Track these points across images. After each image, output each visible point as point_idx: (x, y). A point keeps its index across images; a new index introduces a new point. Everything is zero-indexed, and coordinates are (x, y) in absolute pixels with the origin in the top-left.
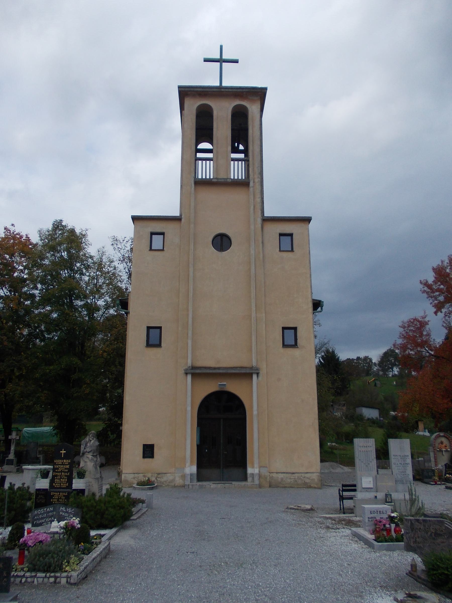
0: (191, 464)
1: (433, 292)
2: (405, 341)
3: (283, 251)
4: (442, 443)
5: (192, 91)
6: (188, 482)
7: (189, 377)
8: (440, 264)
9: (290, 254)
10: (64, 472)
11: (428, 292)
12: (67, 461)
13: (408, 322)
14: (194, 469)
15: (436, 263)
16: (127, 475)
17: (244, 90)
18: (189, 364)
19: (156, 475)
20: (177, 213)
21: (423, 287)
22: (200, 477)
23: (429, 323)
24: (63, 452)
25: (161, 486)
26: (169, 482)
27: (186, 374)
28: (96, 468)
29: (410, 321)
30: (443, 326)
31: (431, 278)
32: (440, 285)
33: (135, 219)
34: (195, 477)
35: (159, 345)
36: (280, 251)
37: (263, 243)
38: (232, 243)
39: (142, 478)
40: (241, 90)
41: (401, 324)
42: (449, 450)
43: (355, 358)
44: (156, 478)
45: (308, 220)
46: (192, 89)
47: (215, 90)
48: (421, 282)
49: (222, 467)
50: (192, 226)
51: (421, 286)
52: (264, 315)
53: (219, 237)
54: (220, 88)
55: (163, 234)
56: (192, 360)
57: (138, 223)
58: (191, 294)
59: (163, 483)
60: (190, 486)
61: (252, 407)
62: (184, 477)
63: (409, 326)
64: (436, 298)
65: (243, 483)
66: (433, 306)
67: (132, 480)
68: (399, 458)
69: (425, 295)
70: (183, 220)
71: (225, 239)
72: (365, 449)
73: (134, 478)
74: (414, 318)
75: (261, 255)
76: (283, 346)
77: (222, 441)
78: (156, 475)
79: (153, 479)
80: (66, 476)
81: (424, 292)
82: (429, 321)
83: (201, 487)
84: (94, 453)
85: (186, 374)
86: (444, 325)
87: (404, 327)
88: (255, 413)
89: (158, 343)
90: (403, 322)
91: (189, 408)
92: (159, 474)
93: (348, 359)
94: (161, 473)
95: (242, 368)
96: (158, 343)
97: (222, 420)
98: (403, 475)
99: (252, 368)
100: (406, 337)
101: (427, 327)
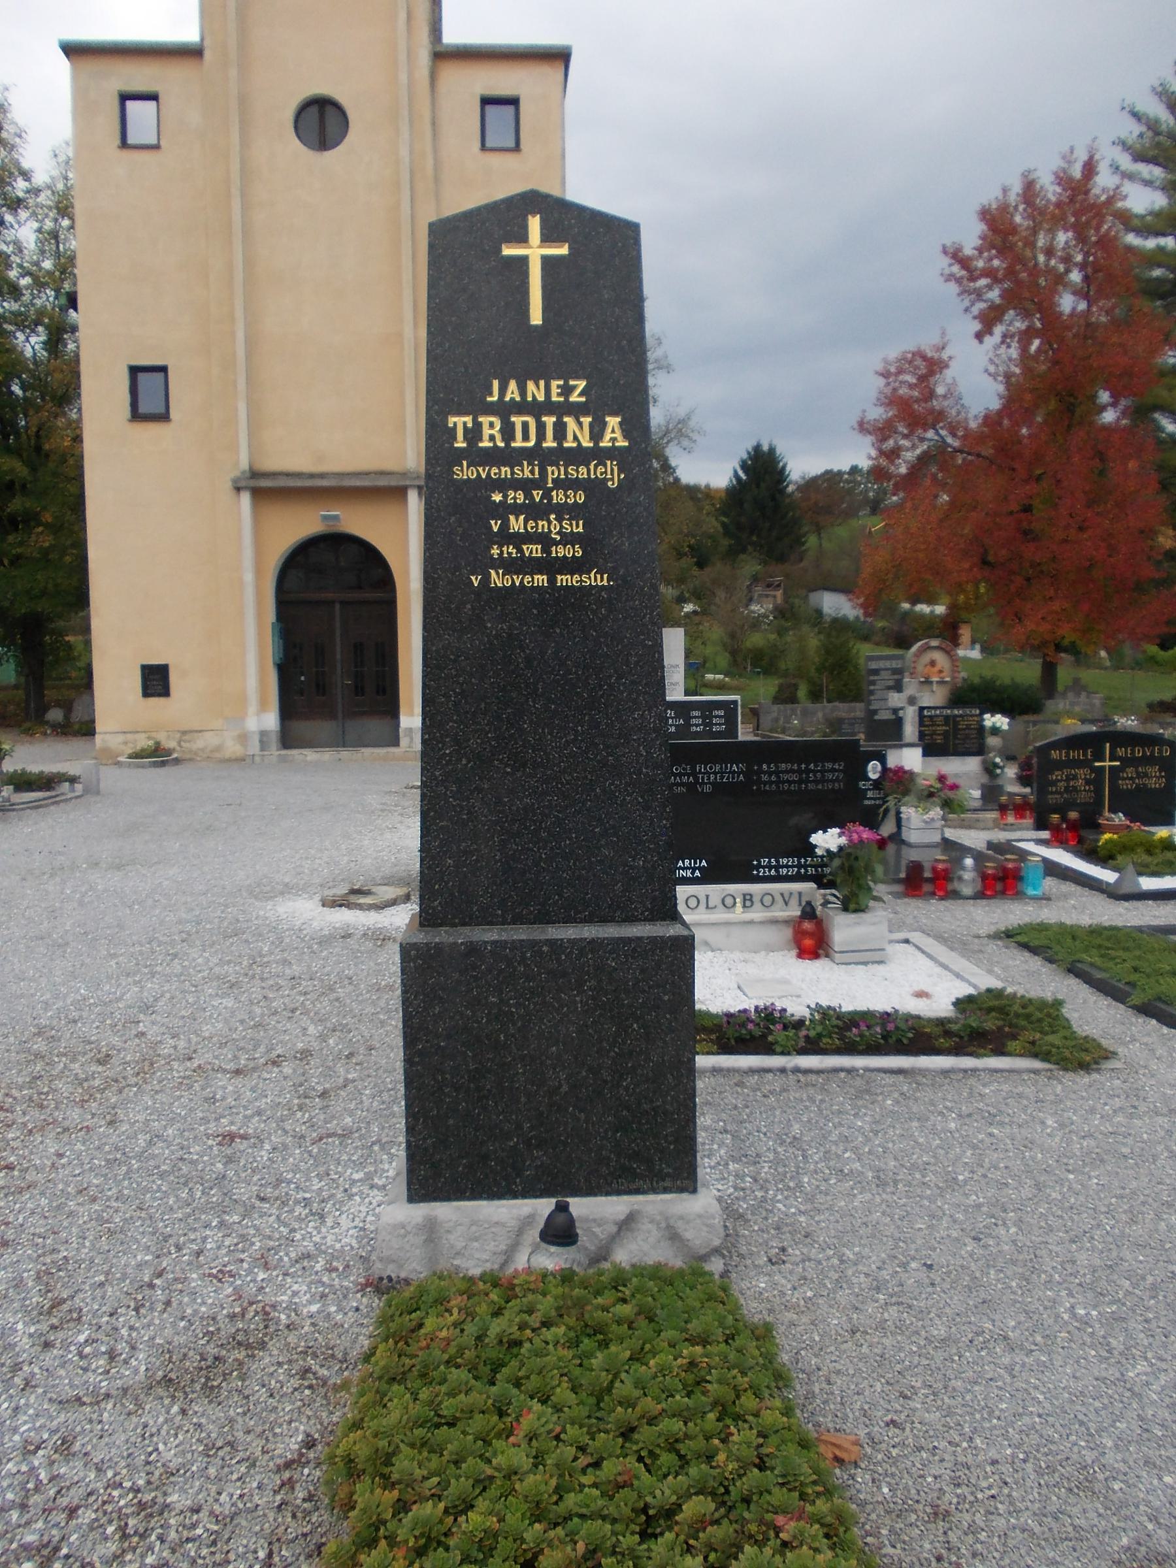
0: (263, 706)
1: (973, 279)
2: (890, 414)
4: (933, 663)
6: (254, 747)
7: (246, 499)
8: (1001, 197)
9: (510, 160)
11: (962, 278)
13: (899, 360)
14: (271, 720)
15: (990, 196)
16: (107, 737)
18: (244, 464)
19: (178, 735)
20: (190, 34)
21: (950, 265)
22: (288, 739)
23: (952, 363)
25: (191, 760)
26: (212, 751)
27: (238, 489)
29: (904, 359)
30: (986, 371)
31: (970, 235)
32: (991, 259)
33: (72, 50)
34: (274, 740)
35: (164, 417)
36: (483, 147)
37: (434, 124)
38: (351, 124)
39: (143, 742)
41: (880, 367)
42: (948, 679)
43: (846, 468)
45: (560, 57)
48: (945, 251)
49: (340, 715)
50: (233, 72)
51: (946, 261)
53: (314, 110)
55: (153, 97)
56: (251, 454)
57: (92, 65)
58: (239, 276)
60: (257, 759)
61: (407, 572)
62: (243, 738)
63: (900, 371)
64: (979, 294)
65: (393, 750)
66: (975, 318)
67: (123, 747)
69: (953, 288)
70: (207, 54)
71: (330, 110)
73: (126, 743)
74: (916, 349)
75: (430, 162)
77: (338, 656)
78: (178, 735)
79: (171, 744)
81: (950, 277)
82: (950, 358)
83: (282, 759)
85: (238, 489)
86: (992, 369)
87: (885, 375)
89: (163, 410)
90: (885, 361)
91: (249, 577)
92: (184, 733)
93: (827, 472)
94: (191, 732)
95: (382, 473)
96: (163, 410)
97: (337, 606)
99: (404, 475)
100: (893, 400)
101: (949, 374)
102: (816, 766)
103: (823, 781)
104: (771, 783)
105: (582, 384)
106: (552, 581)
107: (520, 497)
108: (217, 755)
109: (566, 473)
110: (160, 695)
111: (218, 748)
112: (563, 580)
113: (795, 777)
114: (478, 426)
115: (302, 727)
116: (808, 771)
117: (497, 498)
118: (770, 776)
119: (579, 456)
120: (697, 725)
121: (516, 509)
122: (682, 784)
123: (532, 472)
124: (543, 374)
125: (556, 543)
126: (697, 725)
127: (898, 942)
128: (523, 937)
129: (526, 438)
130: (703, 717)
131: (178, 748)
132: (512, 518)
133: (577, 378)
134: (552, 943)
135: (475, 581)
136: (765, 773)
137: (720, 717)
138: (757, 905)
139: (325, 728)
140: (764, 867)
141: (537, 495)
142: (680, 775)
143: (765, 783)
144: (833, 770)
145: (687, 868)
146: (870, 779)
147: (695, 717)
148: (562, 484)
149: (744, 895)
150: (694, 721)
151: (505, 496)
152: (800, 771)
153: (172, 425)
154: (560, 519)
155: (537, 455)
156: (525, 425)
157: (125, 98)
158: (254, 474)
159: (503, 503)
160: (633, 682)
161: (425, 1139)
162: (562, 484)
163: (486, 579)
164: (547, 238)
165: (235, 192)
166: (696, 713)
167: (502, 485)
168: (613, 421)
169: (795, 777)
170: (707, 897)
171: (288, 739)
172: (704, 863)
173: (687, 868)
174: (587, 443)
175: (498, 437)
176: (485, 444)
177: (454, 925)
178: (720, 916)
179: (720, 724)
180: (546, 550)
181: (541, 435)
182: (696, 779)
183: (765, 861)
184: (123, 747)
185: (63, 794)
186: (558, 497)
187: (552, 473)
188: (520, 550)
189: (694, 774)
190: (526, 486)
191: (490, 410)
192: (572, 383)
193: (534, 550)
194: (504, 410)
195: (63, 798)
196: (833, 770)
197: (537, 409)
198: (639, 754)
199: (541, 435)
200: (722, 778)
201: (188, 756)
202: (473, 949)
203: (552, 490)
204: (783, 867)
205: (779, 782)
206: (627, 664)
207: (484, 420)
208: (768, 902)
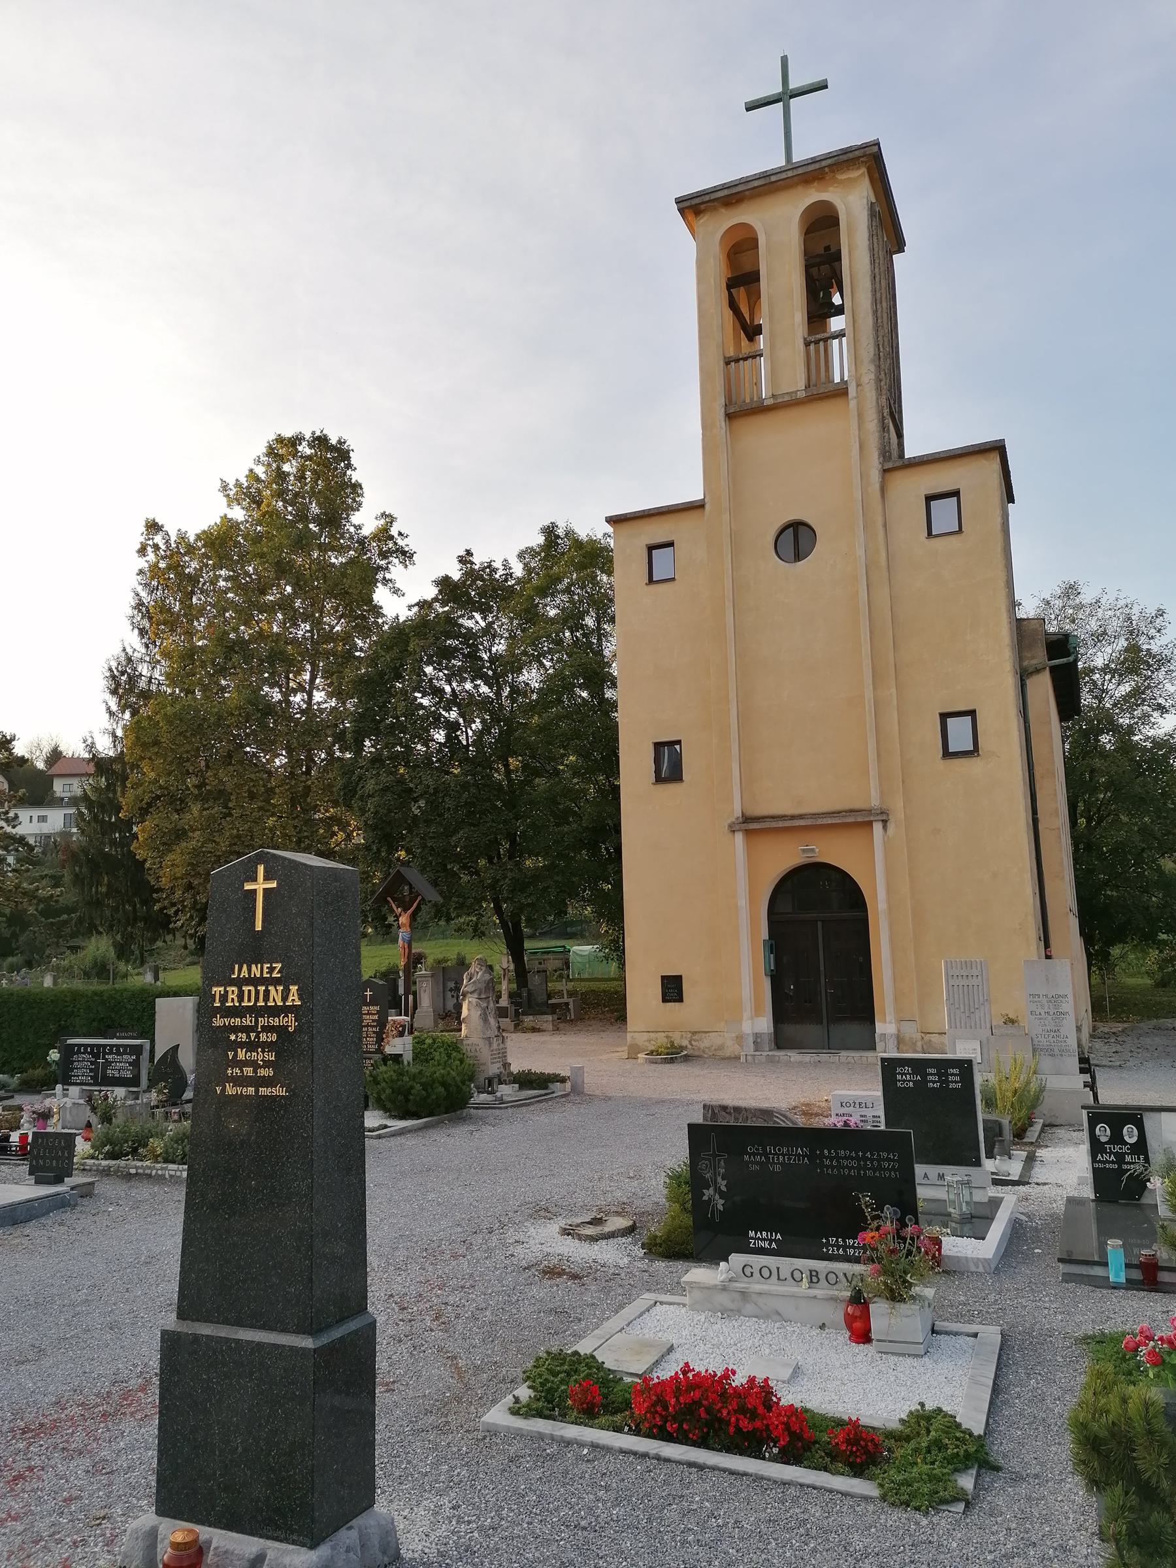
0: (757, 1012)
3: (658, 582)
5: (708, 202)
7: (739, 838)
10: (371, 1026)
12: (375, 1008)
14: (765, 1024)
17: (824, 163)
20: (695, 493)
22: (780, 1041)
24: (368, 993)
26: (715, 1050)
28: (485, 1020)
34: (767, 1043)
37: (885, 525)
40: (817, 166)
44: (690, 1042)
46: (707, 198)
47: (756, 184)
49: (825, 1021)
52: (894, 690)
54: (790, 166)
57: (626, 528)
59: (704, 1052)
62: (740, 1039)
67: (647, 1044)
68: (1045, 1000)
70: (707, 507)
71: (802, 529)
72: (965, 982)
73: (649, 1041)
75: (884, 555)
76: (944, 756)
80: (374, 1032)
83: (771, 1060)
84: (480, 995)
88: (882, 906)
91: (743, 902)
92: (694, 1033)
97: (820, 924)
98: (1053, 1037)
99: (869, 811)
102: (872, 1155)
103: (880, 1168)
104: (833, 1167)
105: (279, 965)
106: (257, 1091)
107: (243, 1037)
108: (720, 1053)
109: (268, 1022)
110: (675, 1001)
111: (721, 1047)
112: (263, 1091)
113: (854, 1163)
114: (226, 992)
115: (790, 1029)
116: (865, 1159)
117: (233, 1037)
118: (831, 1161)
119: (275, 1011)
120: (934, 1082)
121: (241, 1045)
122: (757, 1163)
123: (251, 1021)
124: (258, 960)
125: (261, 1067)
126: (934, 1082)
127: (968, 1335)
128: (223, 1335)
129: (249, 1000)
130: (939, 1074)
131: (690, 1046)
132: (239, 1050)
133: (277, 962)
134: (237, 1341)
135: (218, 1089)
136: (826, 1158)
137: (955, 1075)
138: (823, 1281)
139: (812, 1031)
140: (832, 1246)
141: (253, 1035)
142: (754, 1154)
143: (828, 1167)
144: (888, 1160)
145: (765, 1240)
146: (1126, 1143)
147: (931, 1074)
148: (268, 1029)
149: (811, 1271)
150: (930, 1078)
151: (237, 1037)
152: (857, 1158)
153: (684, 784)
154: (263, 1052)
155: (255, 1011)
156: (249, 991)
157: (651, 548)
158: (747, 819)
159: (235, 1041)
160: (295, 1161)
161: (165, 1470)
162: (268, 1029)
163: (224, 1090)
164: (267, 878)
165: (729, 605)
166: (933, 1071)
167: (235, 1029)
168: (294, 988)
169: (854, 1163)
170: (778, 1268)
171: (780, 1041)
172: (779, 1237)
173: (765, 1240)
174: (280, 1003)
175: (236, 999)
176: (229, 1004)
177: (193, 1320)
178: (789, 1288)
179: (956, 1082)
180: (255, 1071)
181: (257, 999)
182: (767, 1158)
183: (833, 1240)
184: (647, 1044)
185: (553, 1093)
186: (263, 1037)
187: (262, 1021)
188: (242, 1071)
189: (766, 1155)
190: (247, 1030)
191: (233, 982)
192: (274, 965)
193: (248, 1071)
194: (240, 983)
195: (555, 1095)
196: (888, 1160)
197: (254, 982)
198: (295, 1212)
199: (257, 999)
200: (789, 1159)
201: (697, 1053)
202: (196, 1338)
203: (260, 1032)
204: (850, 1247)
205: (840, 1167)
206: (292, 1148)
207: (230, 989)
208: (832, 1280)
